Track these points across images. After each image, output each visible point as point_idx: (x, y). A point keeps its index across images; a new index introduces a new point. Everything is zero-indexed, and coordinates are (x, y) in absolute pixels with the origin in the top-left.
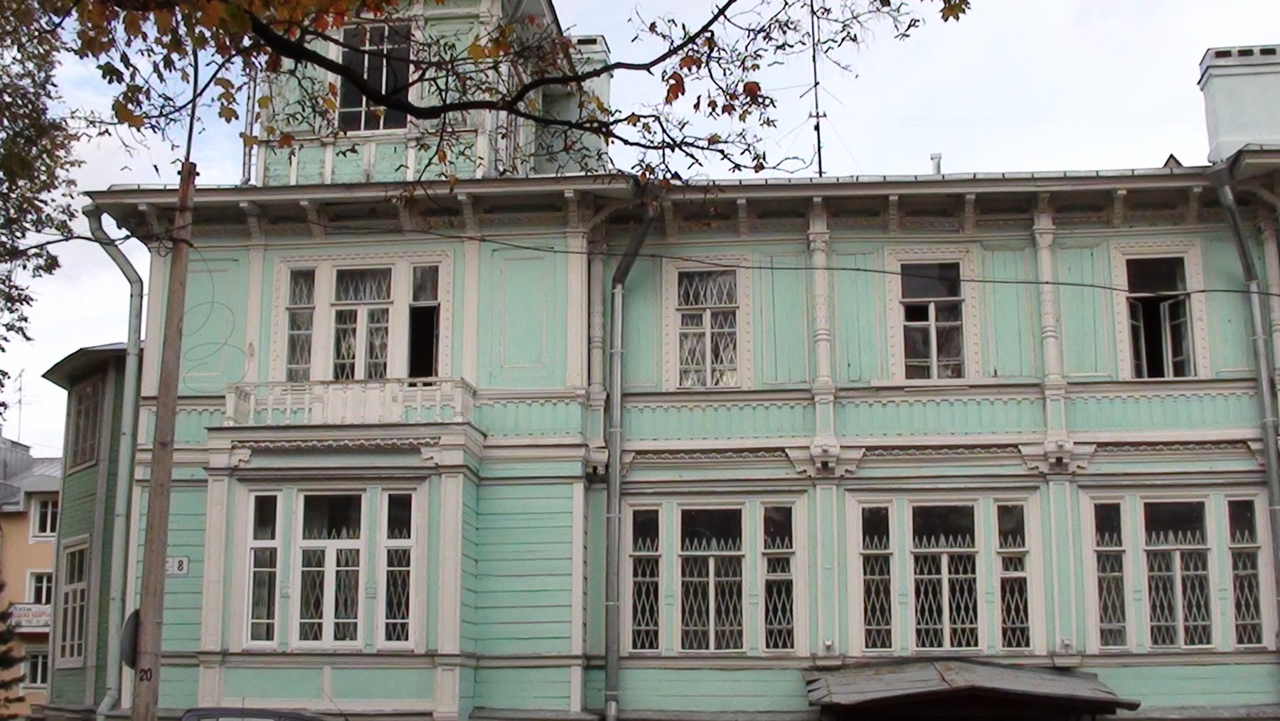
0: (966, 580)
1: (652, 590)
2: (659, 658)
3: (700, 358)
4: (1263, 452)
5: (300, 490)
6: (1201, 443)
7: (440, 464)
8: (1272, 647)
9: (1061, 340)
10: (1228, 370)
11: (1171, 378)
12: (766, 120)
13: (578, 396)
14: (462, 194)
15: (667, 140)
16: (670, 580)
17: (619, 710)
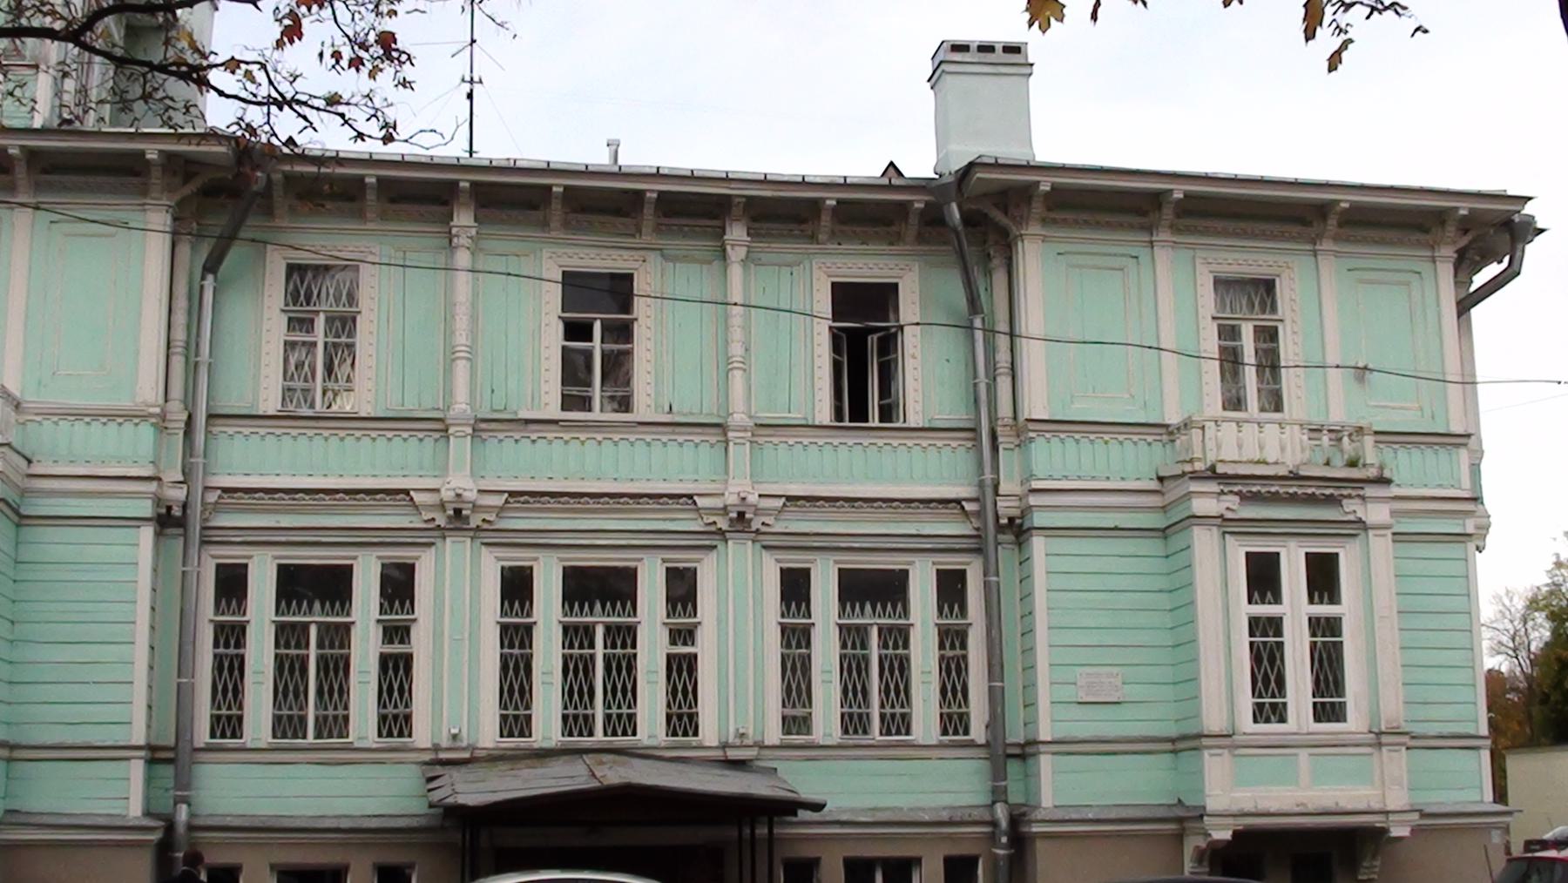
0: (624, 655)
1: (236, 665)
3: (309, 374)
4: (979, 514)
6: (907, 501)
8: (982, 741)
9: (750, 373)
10: (944, 417)
11: (876, 423)
12: (402, 81)
13: (152, 415)
14: (152, 152)
15: (274, 94)
16: (260, 653)
17: (192, 815)
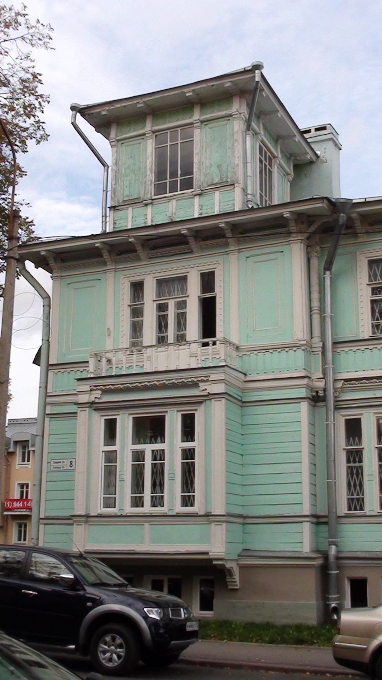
5: (130, 414)
7: (210, 393)
13: (302, 345)
17: (338, 552)
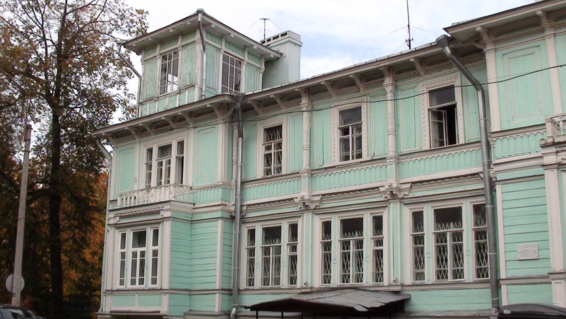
2: (461, 283)
13: (221, 185)
16: (259, 257)
